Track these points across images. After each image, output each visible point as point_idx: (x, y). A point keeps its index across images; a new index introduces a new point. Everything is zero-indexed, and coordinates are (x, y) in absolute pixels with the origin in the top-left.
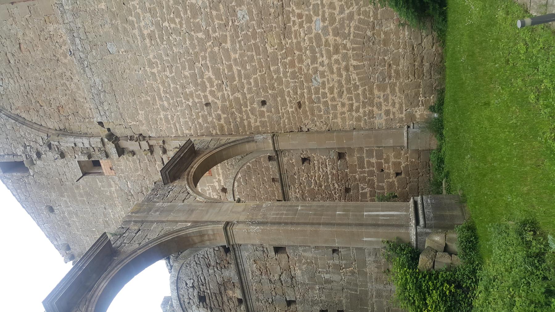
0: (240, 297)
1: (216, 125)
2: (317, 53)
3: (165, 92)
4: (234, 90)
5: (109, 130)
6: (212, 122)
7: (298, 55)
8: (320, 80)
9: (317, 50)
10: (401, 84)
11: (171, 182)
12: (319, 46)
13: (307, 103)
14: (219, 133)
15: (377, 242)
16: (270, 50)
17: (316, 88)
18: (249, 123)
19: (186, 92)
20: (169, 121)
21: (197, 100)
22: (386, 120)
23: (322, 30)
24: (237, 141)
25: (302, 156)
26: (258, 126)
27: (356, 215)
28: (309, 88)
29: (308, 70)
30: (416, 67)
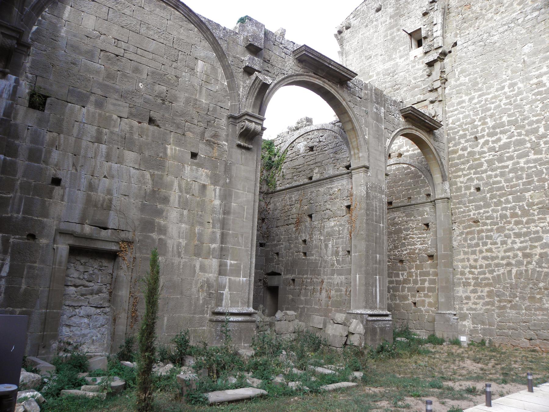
0: (314, 179)
1: (458, 147)
2: (524, 237)
3: (486, 100)
4: (490, 162)
5: (450, 52)
6: (460, 143)
7: (523, 221)
8: (498, 241)
9: (527, 238)
10: (494, 310)
11: (403, 116)
12: (530, 239)
13: (478, 229)
14: (450, 149)
15: (355, 285)
16: (527, 195)
17: (491, 236)
18: (460, 177)
19: (487, 119)
20: (460, 104)
21: (479, 129)
22: (461, 296)
23: (545, 243)
24: (443, 167)
25: (430, 223)
26: (457, 184)
27: (376, 270)
28: (491, 230)
29: (508, 230)
30: (508, 324)
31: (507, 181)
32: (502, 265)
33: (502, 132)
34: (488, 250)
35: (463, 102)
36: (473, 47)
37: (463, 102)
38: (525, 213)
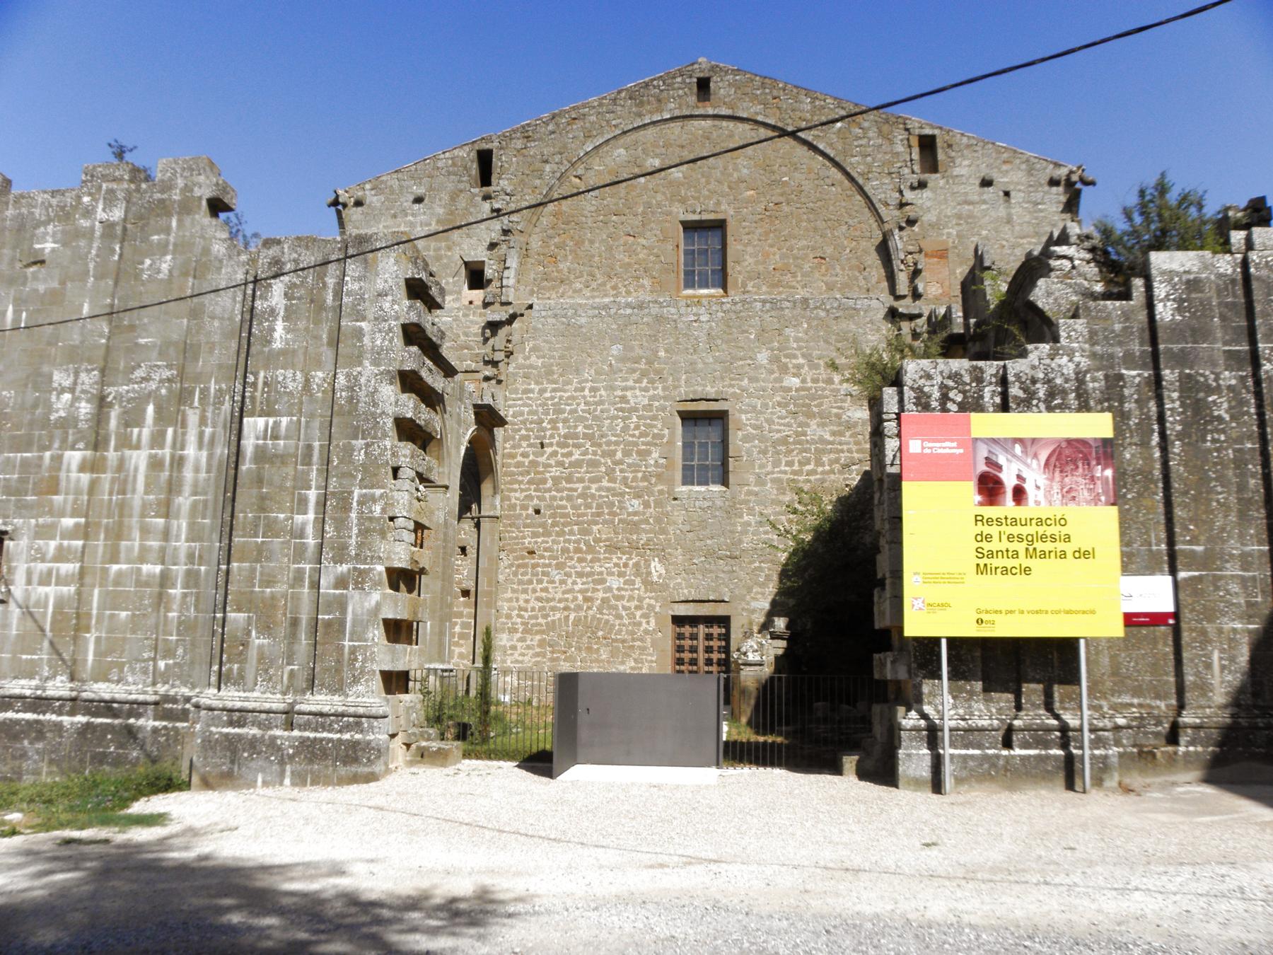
3: (561, 398)
4: (556, 480)
16: (595, 528)
18: (516, 491)
28: (549, 565)
31: (573, 507)
32: (559, 609)
33: (575, 446)
34: (545, 590)
35: (531, 391)
36: (554, 321)
37: (531, 391)
38: (591, 549)
